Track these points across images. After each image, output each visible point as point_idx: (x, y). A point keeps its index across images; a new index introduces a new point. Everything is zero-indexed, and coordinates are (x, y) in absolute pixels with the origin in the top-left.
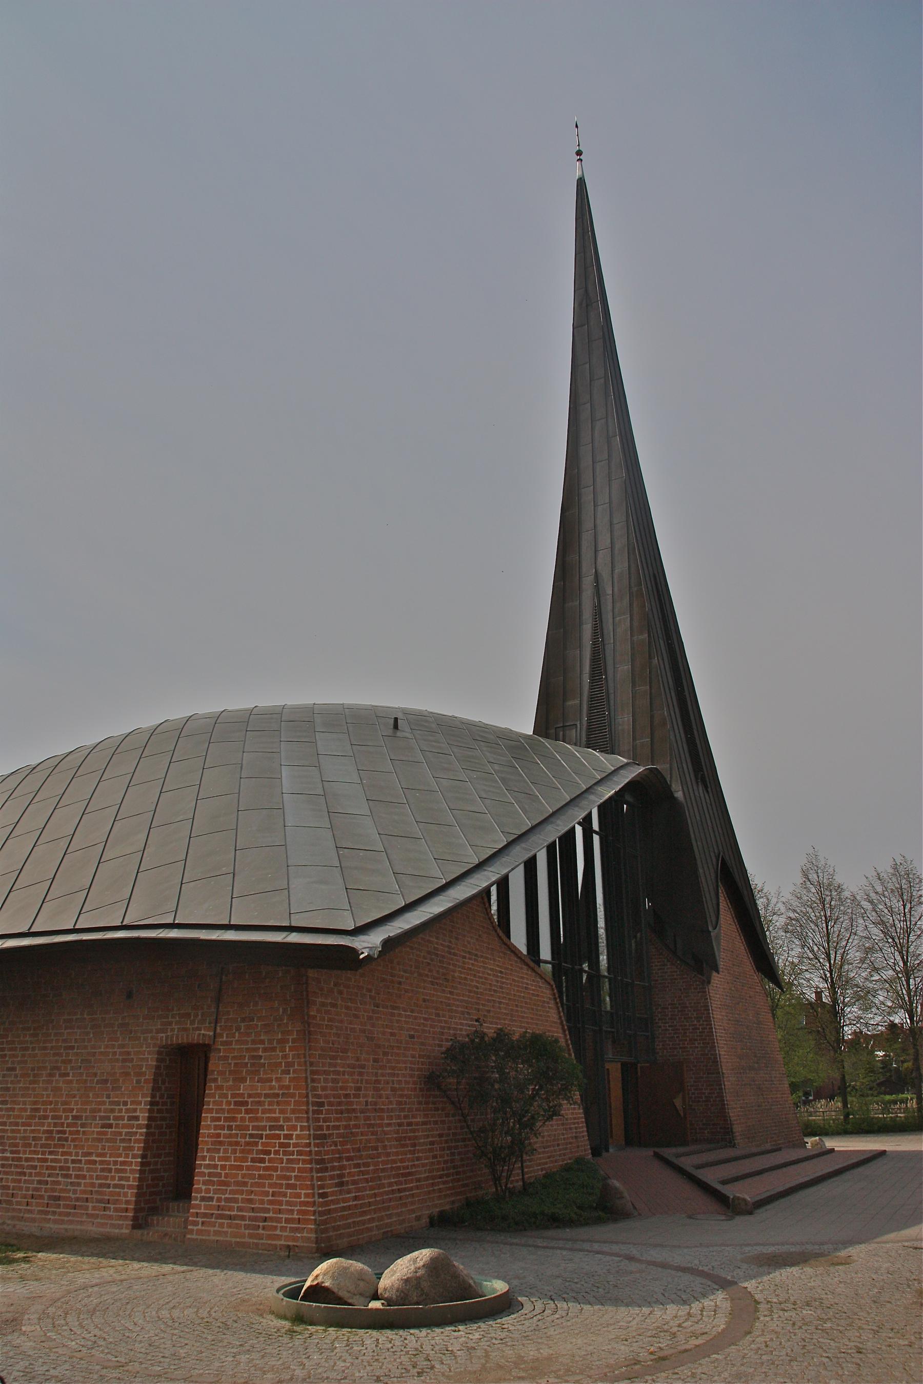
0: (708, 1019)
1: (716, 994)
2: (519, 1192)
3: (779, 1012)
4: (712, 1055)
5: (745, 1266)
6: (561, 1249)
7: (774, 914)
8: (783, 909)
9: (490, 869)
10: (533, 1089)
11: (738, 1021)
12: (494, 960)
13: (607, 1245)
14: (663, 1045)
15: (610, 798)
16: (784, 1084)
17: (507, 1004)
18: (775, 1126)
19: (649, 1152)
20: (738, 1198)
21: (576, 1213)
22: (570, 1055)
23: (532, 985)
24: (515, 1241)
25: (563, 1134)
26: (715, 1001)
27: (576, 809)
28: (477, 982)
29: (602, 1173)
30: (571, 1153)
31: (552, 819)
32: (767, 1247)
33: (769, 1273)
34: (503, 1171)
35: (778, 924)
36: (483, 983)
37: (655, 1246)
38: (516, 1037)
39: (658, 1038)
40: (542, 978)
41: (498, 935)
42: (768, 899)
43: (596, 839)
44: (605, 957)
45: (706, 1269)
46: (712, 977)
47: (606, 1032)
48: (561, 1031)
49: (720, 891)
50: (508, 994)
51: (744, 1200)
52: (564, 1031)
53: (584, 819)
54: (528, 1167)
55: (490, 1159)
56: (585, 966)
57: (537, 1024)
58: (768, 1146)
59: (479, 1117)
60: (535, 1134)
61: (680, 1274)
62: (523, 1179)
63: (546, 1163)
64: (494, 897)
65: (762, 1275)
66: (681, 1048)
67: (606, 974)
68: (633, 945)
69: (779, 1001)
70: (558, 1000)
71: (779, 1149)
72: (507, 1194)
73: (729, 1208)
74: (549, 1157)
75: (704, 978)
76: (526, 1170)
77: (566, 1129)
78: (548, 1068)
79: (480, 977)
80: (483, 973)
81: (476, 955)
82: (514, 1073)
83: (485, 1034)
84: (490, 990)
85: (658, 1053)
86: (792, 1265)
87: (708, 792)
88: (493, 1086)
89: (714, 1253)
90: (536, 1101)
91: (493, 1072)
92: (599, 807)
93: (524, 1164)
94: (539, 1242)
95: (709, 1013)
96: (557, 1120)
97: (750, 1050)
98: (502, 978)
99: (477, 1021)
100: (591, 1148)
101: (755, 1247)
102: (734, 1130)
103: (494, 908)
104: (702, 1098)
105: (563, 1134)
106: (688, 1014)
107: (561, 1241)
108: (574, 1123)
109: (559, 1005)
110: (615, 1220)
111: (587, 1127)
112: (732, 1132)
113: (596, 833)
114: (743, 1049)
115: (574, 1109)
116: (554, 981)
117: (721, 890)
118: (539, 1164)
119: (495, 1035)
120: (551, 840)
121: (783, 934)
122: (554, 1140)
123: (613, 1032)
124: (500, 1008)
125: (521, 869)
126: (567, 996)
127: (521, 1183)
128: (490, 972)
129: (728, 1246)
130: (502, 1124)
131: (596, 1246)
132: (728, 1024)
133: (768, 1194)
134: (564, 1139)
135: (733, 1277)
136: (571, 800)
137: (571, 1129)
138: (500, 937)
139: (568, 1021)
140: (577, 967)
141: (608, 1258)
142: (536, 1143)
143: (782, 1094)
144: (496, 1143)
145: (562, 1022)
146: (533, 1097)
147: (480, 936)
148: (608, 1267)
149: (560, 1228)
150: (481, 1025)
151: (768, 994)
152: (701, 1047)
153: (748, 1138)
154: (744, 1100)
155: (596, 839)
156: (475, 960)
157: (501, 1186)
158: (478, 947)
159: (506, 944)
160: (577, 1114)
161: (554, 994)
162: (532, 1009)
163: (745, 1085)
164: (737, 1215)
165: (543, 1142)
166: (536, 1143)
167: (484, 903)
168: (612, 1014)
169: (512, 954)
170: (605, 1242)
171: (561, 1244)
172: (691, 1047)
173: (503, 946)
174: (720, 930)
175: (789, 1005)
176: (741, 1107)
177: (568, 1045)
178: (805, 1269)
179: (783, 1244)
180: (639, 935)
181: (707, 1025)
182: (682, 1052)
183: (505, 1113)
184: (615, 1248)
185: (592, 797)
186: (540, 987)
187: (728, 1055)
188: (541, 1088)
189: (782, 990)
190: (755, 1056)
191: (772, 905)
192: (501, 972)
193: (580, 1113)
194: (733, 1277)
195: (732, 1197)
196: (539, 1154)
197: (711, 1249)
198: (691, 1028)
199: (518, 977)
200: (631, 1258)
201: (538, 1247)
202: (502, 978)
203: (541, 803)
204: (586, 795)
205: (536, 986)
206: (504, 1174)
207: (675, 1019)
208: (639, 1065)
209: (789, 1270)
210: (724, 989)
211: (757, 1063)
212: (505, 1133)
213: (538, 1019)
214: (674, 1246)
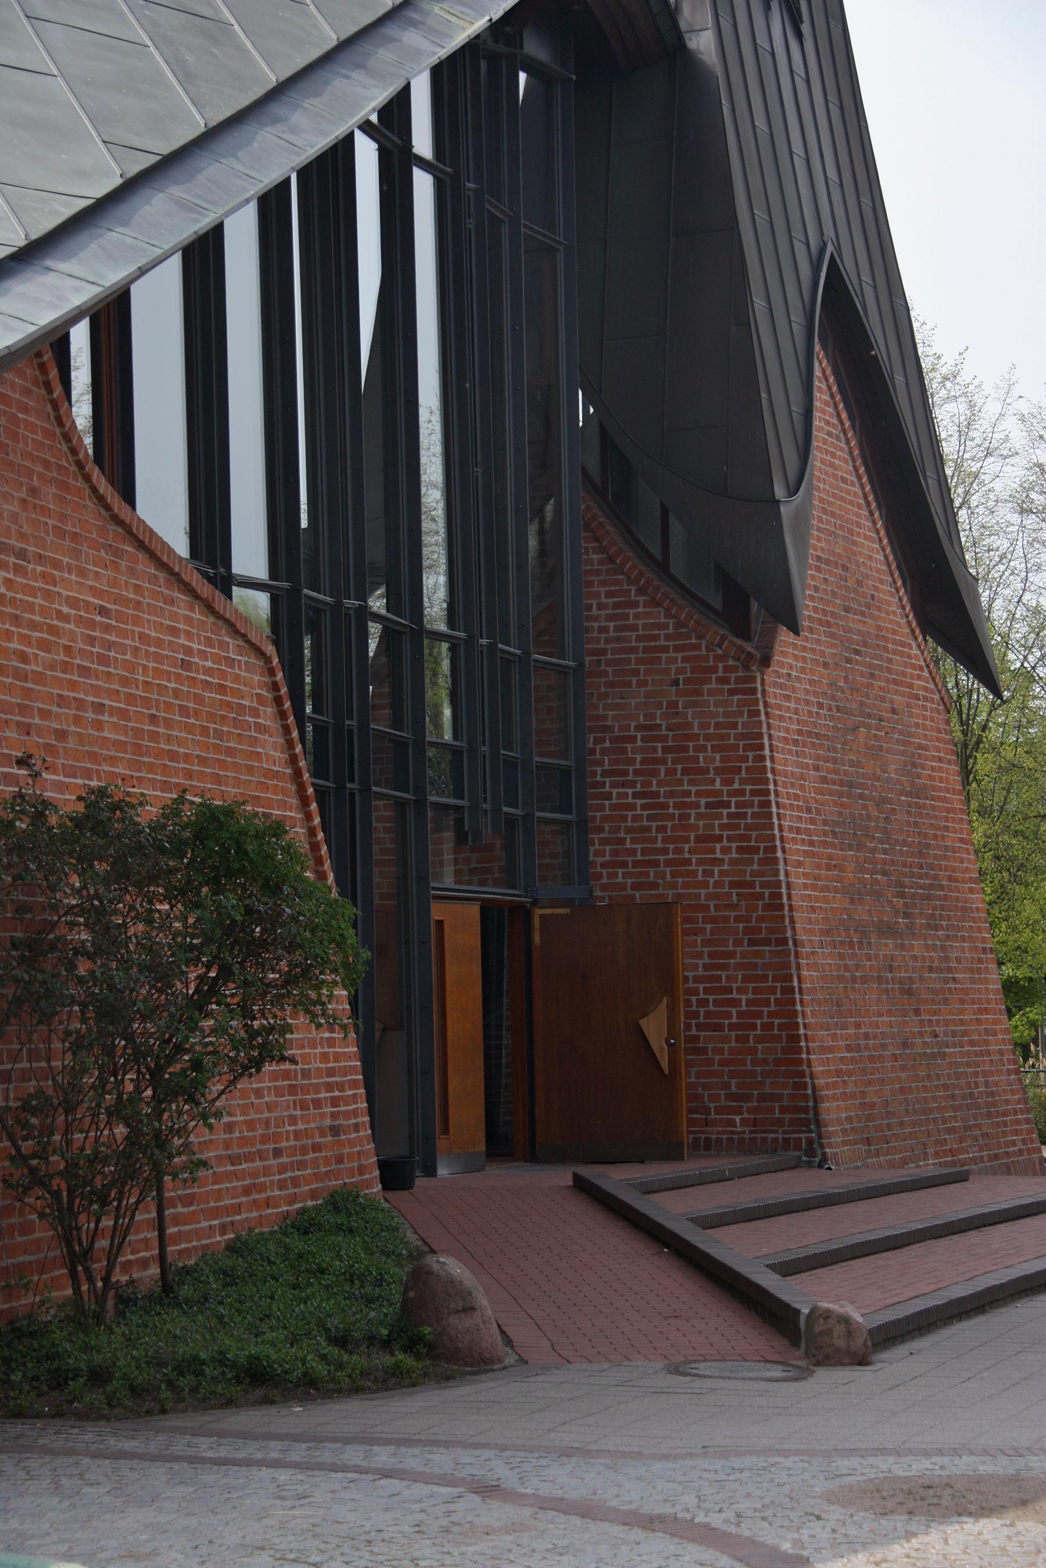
0: (758, 776)
1: (788, 698)
2: (150, 1297)
3: (983, 764)
4: (764, 885)
5: (835, 1513)
6: (275, 1464)
7: (989, 454)
8: (1018, 438)
9: (63, 266)
10: (201, 979)
11: (851, 785)
12: (82, 572)
13: (417, 1451)
14: (615, 853)
15: (472, 47)
16: (986, 981)
17: (123, 714)
18: (955, 1109)
19: (562, 1176)
20: (827, 1315)
21: (323, 1357)
22: (322, 876)
23: (203, 655)
24: (129, 1445)
25: (293, 1120)
26: (781, 718)
27: (357, 75)
28: (25, 639)
29: (411, 1236)
30: (317, 1177)
31: (276, 109)
32: (907, 1459)
33: (909, 1535)
34: (95, 1234)
35: (998, 485)
36: (43, 645)
37: (567, 1452)
38: (149, 814)
39: (601, 830)
40: (235, 632)
41: (94, 489)
42: (971, 406)
43: (423, 184)
44: (442, 579)
45: (716, 1520)
46: (777, 647)
47: (436, 805)
48: (294, 801)
49: (818, 373)
50: (125, 681)
51: (845, 1320)
52: (304, 801)
53: (384, 112)
54: (177, 1220)
55: (57, 1195)
56: (377, 603)
57: (217, 779)
58: (929, 1167)
59: (25, 1065)
60: (204, 1117)
61: (637, 1534)
62: (162, 1257)
63: (237, 1209)
64: (81, 376)
65: (886, 1538)
66: (668, 863)
67: (443, 627)
68: (533, 542)
69: (984, 728)
70: (287, 705)
71: (962, 1178)
72: (110, 1303)
73: (795, 1343)
74: (247, 1191)
75: (749, 647)
76: (171, 1230)
77: (304, 1106)
78: (249, 911)
79: (34, 626)
80: (44, 611)
81: (22, 554)
82: (141, 927)
83: (46, 804)
84: (66, 667)
85: (599, 876)
86: (985, 1511)
87: (799, 35)
88: (72, 966)
89: (746, 1474)
90: (208, 1015)
91: (72, 925)
92: (438, 73)
93: (169, 1212)
94: (205, 1446)
95: (762, 758)
96: (274, 1076)
97: (885, 873)
98: (107, 628)
99: (21, 762)
100: (382, 1165)
101: (871, 1460)
102: (824, 1116)
103: (82, 412)
104: (729, 1015)
105: (293, 1120)
106: (696, 759)
107: (273, 1444)
108: (329, 1087)
109: (291, 719)
110: (447, 1378)
111: (370, 1099)
112: (818, 1123)
113: (424, 165)
114: (862, 870)
115: (331, 1042)
116: (276, 643)
117: (821, 366)
118: (215, 1213)
119: (81, 808)
120: (269, 179)
121: (1015, 518)
122: (265, 1139)
123: (458, 809)
124: (99, 725)
125: (172, 270)
126: (316, 674)
127: (154, 1270)
128: (65, 609)
129: (786, 1454)
130: (101, 1087)
131: (383, 1456)
132: (820, 791)
133: (920, 1305)
134: (297, 1134)
135: (798, 1543)
136: (345, 45)
137: (318, 1103)
138: (101, 500)
139: (319, 770)
140: (352, 603)
141: (419, 1489)
142: (205, 1145)
143: (980, 1011)
144: (76, 1145)
145: (298, 773)
146: (199, 1004)
147: (33, 491)
148: (419, 1516)
149: (272, 1402)
150: (35, 776)
151: (949, 704)
152: (732, 862)
153: (868, 1141)
154: (858, 1026)
155: (423, 184)
156: (17, 569)
157: (91, 1280)
158: (26, 530)
159: (120, 522)
160: (337, 1057)
161: (275, 687)
162: (205, 731)
163: (864, 979)
164: (818, 1364)
165: (227, 1145)
166: (205, 1145)
167: (48, 387)
168: (456, 753)
169: (141, 556)
170: (408, 1442)
171: (274, 1450)
172: (700, 862)
173: (112, 527)
174: (809, 495)
175: (1016, 744)
176: (849, 1048)
177: (315, 847)
178: (1020, 1526)
179: (956, 1452)
180: (549, 508)
181: (754, 793)
182: (674, 875)
183: (110, 1051)
184: (442, 1460)
185: (412, 38)
186: (231, 662)
187: (814, 887)
188: (226, 973)
189: (998, 694)
190: (902, 895)
191: (983, 424)
192: (103, 611)
193: (348, 1057)
194: (798, 1543)
195: (806, 1311)
196: (217, 1179)
197: (737, 1462)
198: (703, 801)
199: (159, 626)
200: (488, 1490)
201: (202, 1460)
202: (107, 628)
203: (241, 49)
204: (391, 30)
205: (217, 660)
206: (103, 1243)
207: (655, 773)
208: (539, 912)
209: (971, 1526)
210: (811, 682)
211: (906, 915)
212: (110, 1115)
213: (223, 764)
214: (625, 1455)
